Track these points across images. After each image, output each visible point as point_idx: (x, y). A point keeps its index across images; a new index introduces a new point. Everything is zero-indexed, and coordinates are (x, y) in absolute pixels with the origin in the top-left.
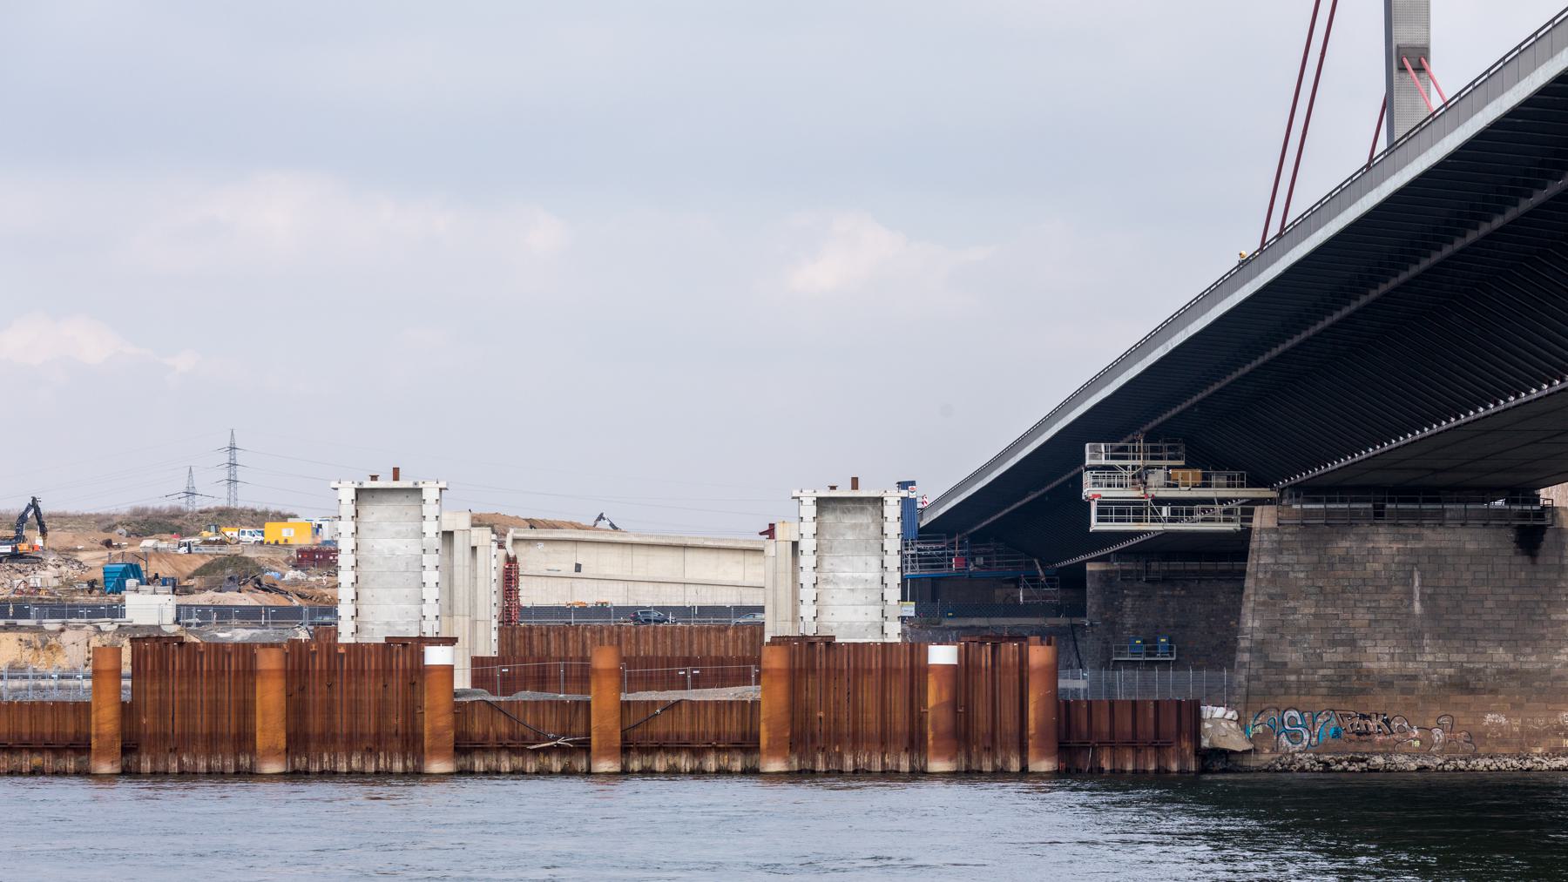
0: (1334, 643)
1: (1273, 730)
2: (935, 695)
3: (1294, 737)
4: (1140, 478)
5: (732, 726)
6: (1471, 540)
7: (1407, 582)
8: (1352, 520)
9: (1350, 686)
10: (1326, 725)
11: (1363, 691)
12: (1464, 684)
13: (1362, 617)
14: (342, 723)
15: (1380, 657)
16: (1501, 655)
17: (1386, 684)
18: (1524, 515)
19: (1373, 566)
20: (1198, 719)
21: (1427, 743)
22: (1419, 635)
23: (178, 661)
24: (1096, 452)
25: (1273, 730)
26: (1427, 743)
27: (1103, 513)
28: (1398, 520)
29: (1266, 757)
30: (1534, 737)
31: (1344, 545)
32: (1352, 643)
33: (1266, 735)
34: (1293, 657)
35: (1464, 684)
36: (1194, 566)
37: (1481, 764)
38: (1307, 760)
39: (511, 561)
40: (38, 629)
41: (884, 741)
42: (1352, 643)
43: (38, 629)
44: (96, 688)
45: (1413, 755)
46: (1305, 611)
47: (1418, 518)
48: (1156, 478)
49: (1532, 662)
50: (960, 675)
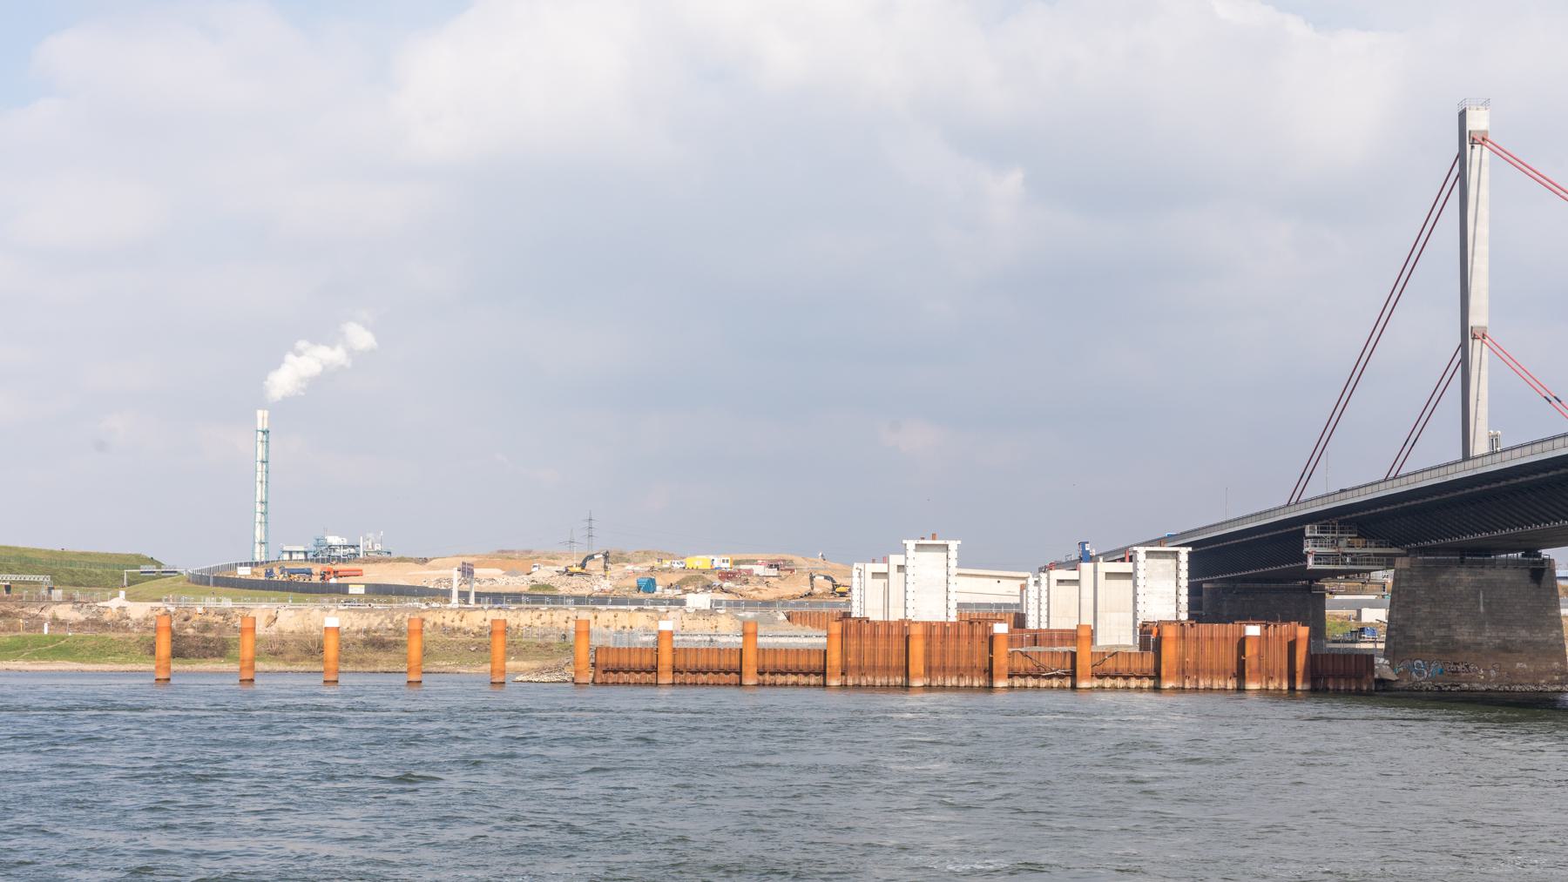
0: (1440, 626)
1: (1408, 670)
2: (1250, 651)
3: (1420, 673)
4: (1335, 543)
5: (815, 662)
6: (1509, 575)
7: (1477, 596)
8: (1447, 565)
9: (1448, 648)
10: (1435, 668)
11: (1455, 651)
12: (1506, 648)
13: (1454, 613)
14: (950, 662)
15: (1464, 634)
16: (1523, 633)
17: (1466, 647)
18: (1535, 563)
19: (1459, 588)
20: (1373, 665)
21: (1487, 677)
22: (1483, 623)
23: (867, 629)
24: (1312, 530)
25: (1408, 670)
26: (1487, 677)
27: (1318, 558)
28: (1471, 565)
29: (1405, 683)
30: (1541, 674)
31: (1444, 577)
32: (1449, 626)
33: (1405, 672)
34: (1419, 633)
35: (1506, 648)
36: (1258, 585)
37: (1518, 688)
38: (1428, 685)
39: (446, 594)
40: (655, 611)
41: (887, 670)
42: (1449, 626)
43: (655, 611)
44: (745, 642)
45: (1482, 683)
46: (1424, 610)
47: (1482, 564)
48: (1342, 543)
49: (1539, 637)
50: (1264, 638)
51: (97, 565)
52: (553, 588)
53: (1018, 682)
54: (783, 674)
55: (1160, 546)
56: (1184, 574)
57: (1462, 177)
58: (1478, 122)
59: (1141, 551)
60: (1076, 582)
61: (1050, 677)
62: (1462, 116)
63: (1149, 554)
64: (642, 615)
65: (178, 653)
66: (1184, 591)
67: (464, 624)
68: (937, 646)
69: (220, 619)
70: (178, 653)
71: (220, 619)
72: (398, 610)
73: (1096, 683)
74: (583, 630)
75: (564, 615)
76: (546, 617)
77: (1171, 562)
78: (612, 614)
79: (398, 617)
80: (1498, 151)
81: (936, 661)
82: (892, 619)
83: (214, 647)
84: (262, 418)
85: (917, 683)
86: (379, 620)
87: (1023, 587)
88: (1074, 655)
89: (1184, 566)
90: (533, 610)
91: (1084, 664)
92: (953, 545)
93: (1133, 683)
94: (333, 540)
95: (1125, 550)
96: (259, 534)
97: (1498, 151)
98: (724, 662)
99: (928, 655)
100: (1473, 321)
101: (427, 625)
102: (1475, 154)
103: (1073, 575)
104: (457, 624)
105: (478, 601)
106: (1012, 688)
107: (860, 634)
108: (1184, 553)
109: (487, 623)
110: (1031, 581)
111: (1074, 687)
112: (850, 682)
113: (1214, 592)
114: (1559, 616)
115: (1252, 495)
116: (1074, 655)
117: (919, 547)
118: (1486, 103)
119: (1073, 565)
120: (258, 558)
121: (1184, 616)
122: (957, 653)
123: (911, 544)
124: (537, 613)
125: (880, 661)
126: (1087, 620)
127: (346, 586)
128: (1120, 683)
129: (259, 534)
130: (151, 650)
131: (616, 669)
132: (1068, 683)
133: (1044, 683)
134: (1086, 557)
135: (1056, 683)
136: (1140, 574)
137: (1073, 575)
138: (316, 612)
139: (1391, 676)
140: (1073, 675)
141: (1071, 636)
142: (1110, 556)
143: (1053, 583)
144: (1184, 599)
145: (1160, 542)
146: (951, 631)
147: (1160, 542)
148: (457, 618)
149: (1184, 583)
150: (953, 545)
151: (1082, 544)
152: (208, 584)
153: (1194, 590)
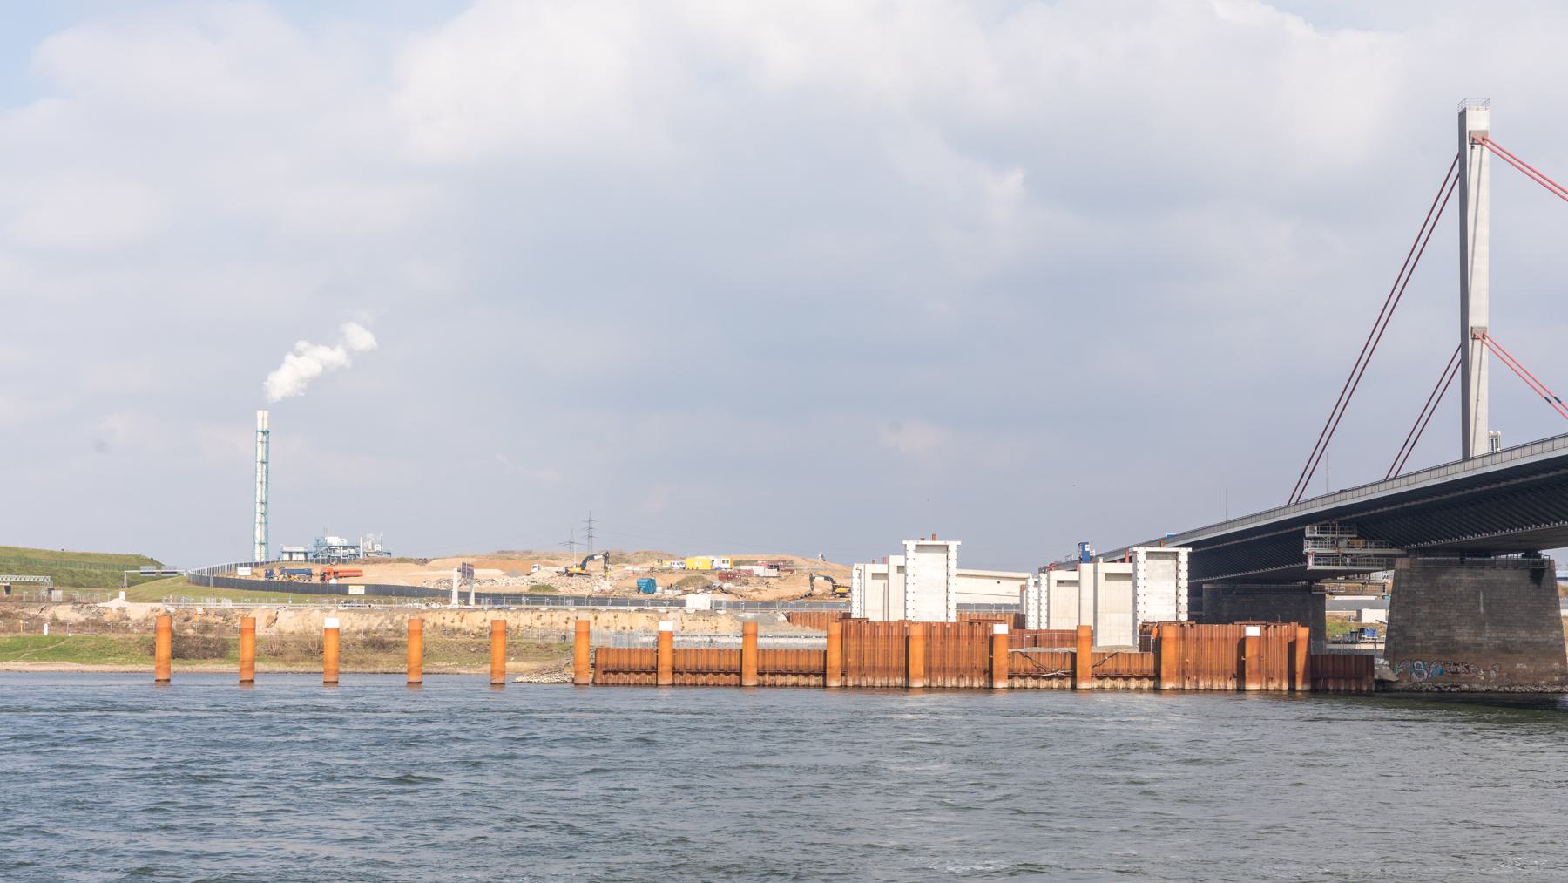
0: (1440, 627)
1: (1408, 671)
2: (1250, 651)
3: (1420, 674)
4: (1335, 543)
5: (815, 662)
6: (1509, 576)
7: (1477, 596)
8: (1447, 566)
9: (1448, 649)
10: (1435, 668)
11: (1455, 652)
12: (1506, 649)
13: (1454, 614)
14: (950, 663)
15: (1464, 634)
16: (1523, 634)
17: (1466, 648)
18: (1535, 564)
19: (1459, 589)
20: (1373, 665)
21: (1487, 678)
22: (1483, 624)
23: (867, 630)
24: (1312, 531)
25: (1408, 671)
26: (1487, 678)
27: (1318, 558)
28: (1471, 566)
29: (1405, 684)
30: (1541, 675)
31: (1444, 578)
32: (1449, 627)
33: (1405, 673)
34: (1419, 634)
35: (1506, 649)
36: (1258, 586)
37: (1518, 689)
38: (1428, 686)
39: (446, 595)
40: (655, 611)
41: (887, 670)
42: (1449, 627)
43: (655, 611)
44: (745, 643)
45: (1482, 683)
46: (1424, 611)
47: (1482, 565)
48: (1342, 544)
49: (1539, 637)
50: (1264, 639)
51: (97, 566)
52: (553, 589)
53: (1018, 683)
54: (783, 674)
55: (1160, 546)
56: (1184, 575)
57: (1462, 177)
58: (1478, 122)
59: (1141, 552)
60: (1076, 583)
61: (1050, 678)
62: (1462, 116)
63: (1149, 555)
64: (642, 616)
65: (178, 654)
66: (1184, 592)
67: (464, 625)
68: (937, 647)
69: (220, 619)
70: (178, 654)
71: (220, 619)
72: (398, 611)
73: (1096, 684)
74: (583, 631)
75: (564, 615)
76: (546, 618)
77: (1171, 563)
78: (612, 615)
79: (398, 618)
80: (1498, 151)
81: (936, 662)
82: (892, 619)
83: (214, 648)
84: (262, 419)
85: (917, 684)
86: (379, 621)
87: (1023, 588)
88: (1074, 655)
89: (1184, 567)
90: (533, 611)
91: (1084, 664)
92: (953, 546)
93: (1133, 684)
94: (333, 540)
95: (1125, 550)
96: (259, 535)
97: (1498, 151)
98: (724, 663)
99: (928, 656)
100: (1473, 322)
101: (427, 626)
102: (1475, 154)
103: (1073, 576)
104: (457, 625)
105: (478, 602)
106: (1012, 688)
107: (860, 635)
108: (1184, 554)
109: (487, 624)
110: (1031, 582)
111: (1074, 688)
112: (850, 683)
113: (1214, 592)
114: (1559, 617)
115: (1252, 496)
116: (1074, 655)
117: (919, 548)
118: (1486, 103)
119: (1073, 566)
120: (258, 559)
121: (1184, 617)
122: (957, 654)
123: (911, 545)
124: (537, 614)
125: (880, 662)
126: (1087, 621)
127: (346, 587)
128: (1120, 684)
129: (259, 535)
130: (151, 650)
131: (616, 669)
132: (1068, 684)
133: (1044, 684)
134: (1086, 558)
135: (1056, 683)
136: (1140, 575)
137: (1073, 576)
138: (316, 613)
139: (1391, 677)
140: (1073, 676)
141: (1071, 637)
142: (1110, 557)
143: (1053, 583)
144: (1184, 600)
145: (1160, 542)
146: (951, 632)
147: (1160, 542)
148: (457, 618)
149: (1184, 583)
150: (953, 546)
151: (1082, 545)
152: (208, 584)
153: (1194, 591)
